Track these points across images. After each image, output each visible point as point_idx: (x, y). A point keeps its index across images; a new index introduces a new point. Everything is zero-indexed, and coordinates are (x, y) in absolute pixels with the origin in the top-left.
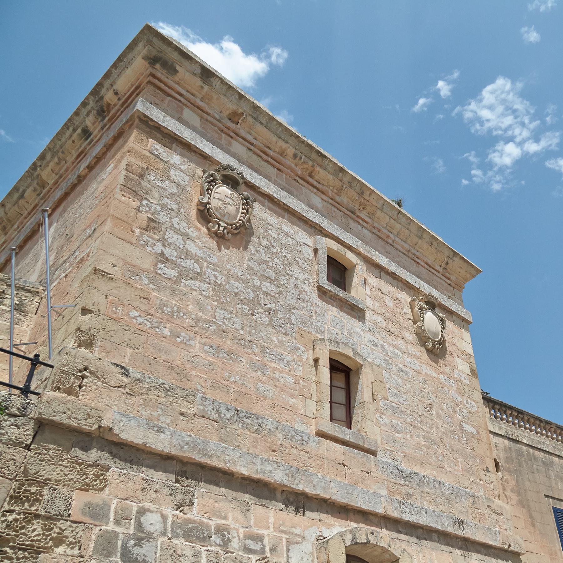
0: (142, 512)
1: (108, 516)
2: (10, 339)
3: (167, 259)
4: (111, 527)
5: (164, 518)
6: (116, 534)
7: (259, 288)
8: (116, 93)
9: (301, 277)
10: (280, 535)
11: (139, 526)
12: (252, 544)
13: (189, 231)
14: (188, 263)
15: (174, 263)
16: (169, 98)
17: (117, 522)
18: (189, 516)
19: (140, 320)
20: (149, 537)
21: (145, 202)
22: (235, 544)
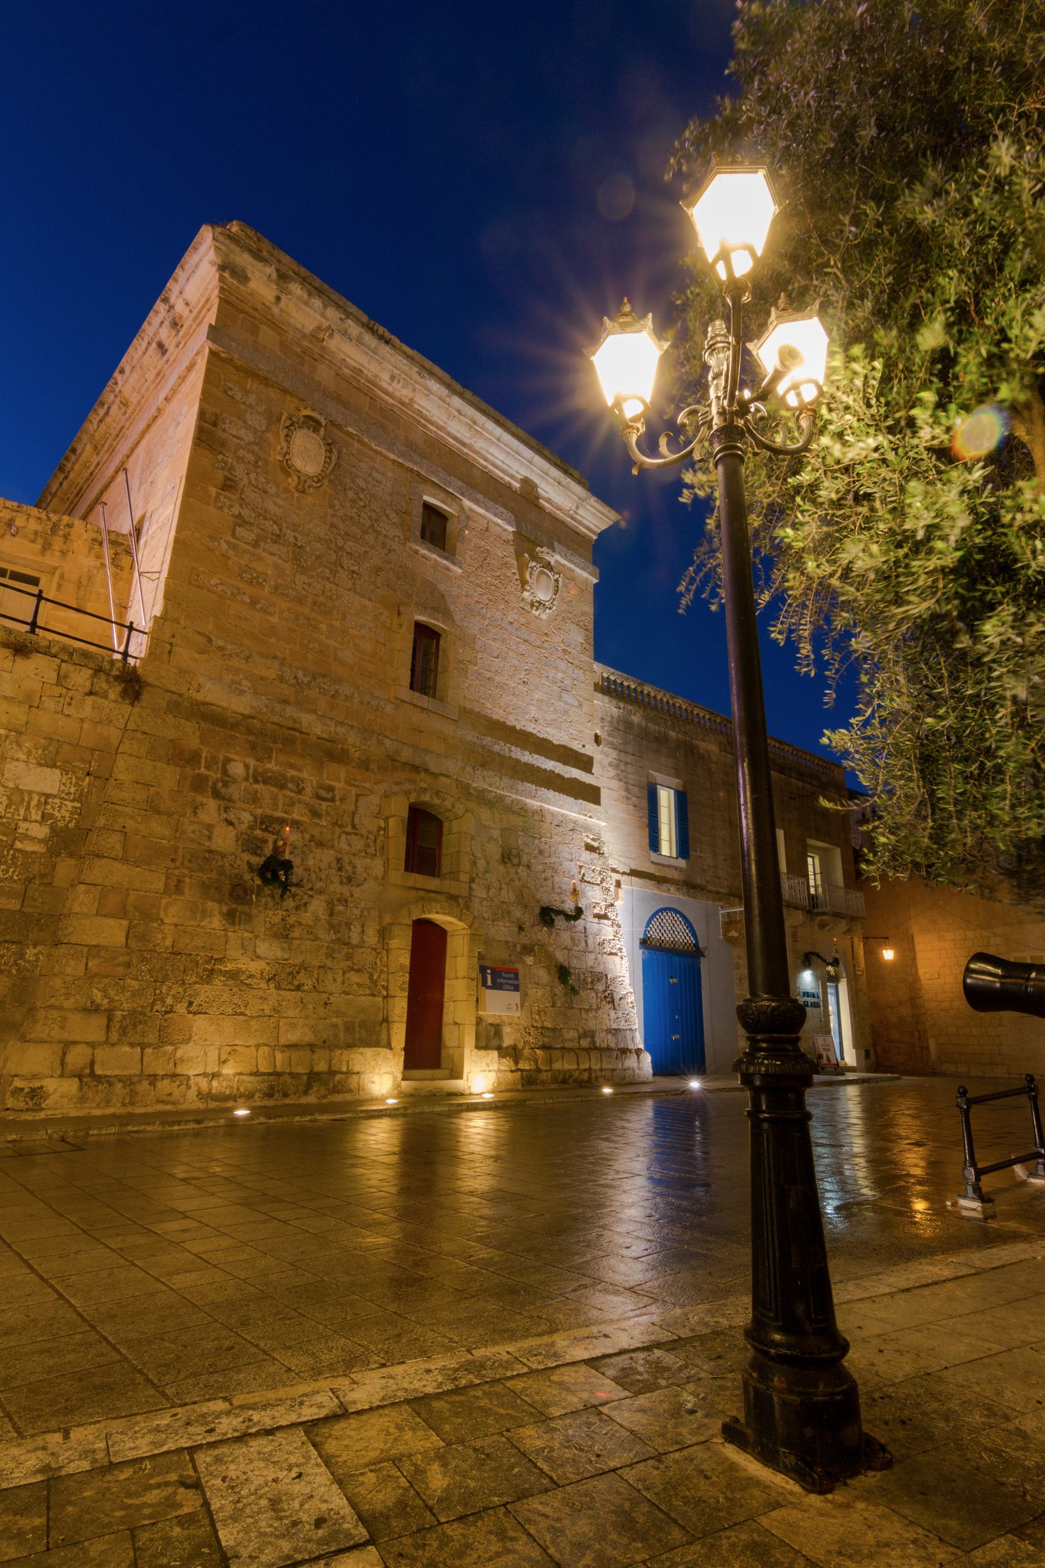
0: (228, 760)
1: (199, 762)
2: (371, 1409)
3: (244, 521)
4: (203, 770)
5: (247, 766)
6: (207, 777)
7: (341, 549)
8: (187, 304)
9: (391, 534)
11: (225, 772)
12: (323, 793)
13: (267, 488)
14: (269, 526)
15: (251, 524)
16: (241, 316)
17: (208, 768)
18: (269, 766)
19: (221, 588)
20: (234, 781)
21: (220, 457)
22: (309, 791)
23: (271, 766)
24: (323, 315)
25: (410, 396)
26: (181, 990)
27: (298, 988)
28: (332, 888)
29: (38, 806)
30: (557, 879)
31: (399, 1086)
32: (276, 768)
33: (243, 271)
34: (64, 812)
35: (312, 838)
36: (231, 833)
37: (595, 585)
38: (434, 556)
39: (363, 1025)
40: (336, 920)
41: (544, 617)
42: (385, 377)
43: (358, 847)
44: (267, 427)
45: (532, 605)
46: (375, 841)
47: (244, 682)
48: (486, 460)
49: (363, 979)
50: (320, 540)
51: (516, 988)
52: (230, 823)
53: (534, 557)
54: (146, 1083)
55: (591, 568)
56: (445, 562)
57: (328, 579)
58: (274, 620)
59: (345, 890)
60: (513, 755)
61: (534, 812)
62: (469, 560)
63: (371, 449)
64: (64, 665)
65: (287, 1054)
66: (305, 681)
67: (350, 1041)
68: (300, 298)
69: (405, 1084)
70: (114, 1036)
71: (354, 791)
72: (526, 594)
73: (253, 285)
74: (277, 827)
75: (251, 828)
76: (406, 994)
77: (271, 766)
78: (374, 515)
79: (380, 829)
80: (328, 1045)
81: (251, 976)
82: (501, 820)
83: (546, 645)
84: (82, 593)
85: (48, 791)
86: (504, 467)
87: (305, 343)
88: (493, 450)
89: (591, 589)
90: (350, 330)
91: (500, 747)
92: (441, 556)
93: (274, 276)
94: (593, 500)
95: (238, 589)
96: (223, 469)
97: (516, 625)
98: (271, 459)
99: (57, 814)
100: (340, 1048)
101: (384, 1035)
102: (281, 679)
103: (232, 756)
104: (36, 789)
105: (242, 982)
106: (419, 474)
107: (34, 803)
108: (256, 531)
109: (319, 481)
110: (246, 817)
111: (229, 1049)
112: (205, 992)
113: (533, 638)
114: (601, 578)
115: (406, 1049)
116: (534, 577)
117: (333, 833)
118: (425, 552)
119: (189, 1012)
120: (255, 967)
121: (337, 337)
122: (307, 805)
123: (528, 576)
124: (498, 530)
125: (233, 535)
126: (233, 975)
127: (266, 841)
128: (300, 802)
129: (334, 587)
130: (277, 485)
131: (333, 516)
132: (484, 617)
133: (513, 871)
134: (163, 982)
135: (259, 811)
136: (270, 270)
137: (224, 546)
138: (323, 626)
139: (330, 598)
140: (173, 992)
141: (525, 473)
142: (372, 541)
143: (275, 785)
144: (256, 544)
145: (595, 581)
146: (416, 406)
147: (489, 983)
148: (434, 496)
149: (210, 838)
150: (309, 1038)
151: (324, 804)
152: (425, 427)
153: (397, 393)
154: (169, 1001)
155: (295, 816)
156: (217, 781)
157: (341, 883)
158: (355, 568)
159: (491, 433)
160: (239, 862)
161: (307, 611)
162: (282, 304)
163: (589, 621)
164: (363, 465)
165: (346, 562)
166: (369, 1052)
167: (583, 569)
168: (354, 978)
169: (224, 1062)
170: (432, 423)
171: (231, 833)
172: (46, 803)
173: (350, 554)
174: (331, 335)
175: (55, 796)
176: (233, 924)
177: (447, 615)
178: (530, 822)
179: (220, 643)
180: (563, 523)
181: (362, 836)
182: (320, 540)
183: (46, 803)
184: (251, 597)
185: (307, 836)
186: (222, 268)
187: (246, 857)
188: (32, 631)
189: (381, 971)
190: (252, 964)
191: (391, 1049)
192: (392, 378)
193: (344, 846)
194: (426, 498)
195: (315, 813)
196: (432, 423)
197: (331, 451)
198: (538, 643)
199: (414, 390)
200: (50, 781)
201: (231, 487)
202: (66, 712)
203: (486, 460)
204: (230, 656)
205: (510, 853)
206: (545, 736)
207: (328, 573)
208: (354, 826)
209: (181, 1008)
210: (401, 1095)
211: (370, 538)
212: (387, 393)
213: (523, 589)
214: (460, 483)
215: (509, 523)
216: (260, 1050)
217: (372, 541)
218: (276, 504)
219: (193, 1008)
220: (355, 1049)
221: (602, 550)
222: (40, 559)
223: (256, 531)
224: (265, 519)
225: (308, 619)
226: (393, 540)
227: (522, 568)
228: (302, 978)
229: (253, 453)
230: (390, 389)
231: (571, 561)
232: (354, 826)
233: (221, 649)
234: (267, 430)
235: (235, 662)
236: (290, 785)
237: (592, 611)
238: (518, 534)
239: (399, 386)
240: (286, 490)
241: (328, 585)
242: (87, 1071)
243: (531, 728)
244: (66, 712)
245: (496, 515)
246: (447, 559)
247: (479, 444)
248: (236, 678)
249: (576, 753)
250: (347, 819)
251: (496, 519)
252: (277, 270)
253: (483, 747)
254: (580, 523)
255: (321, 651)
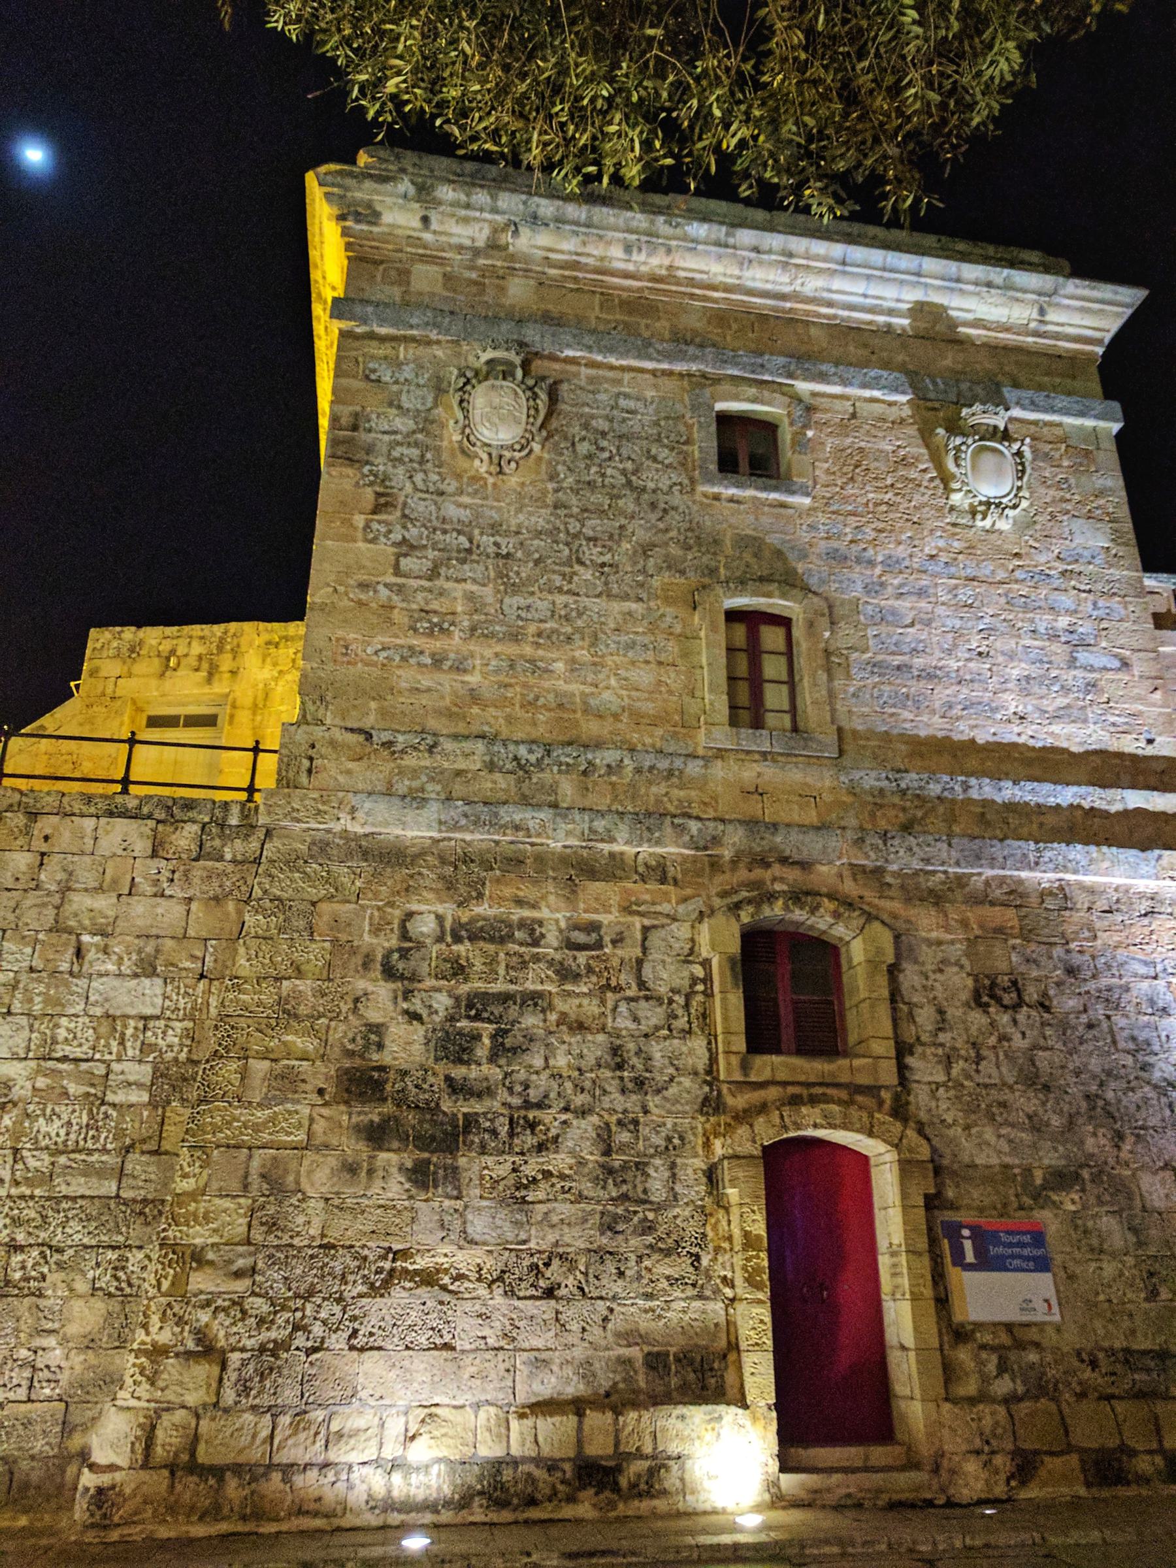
0: (410, 915)
5: (440, 918)
9: (664, 484)
10: (630, 919)
11: (405, 936)
12: (580, 937)
20: (420, 945)
22: (552, 938)
23: (483, 909)
24: (495, 210)
25: (667, 262)
26: (337, 1309)
27: (549, 1293)
28: (606, 1102)
29: (135, 1037)
30: (1119, 1021)
31: (776, 1484)
32: (491, 912)
33: (369, 205)
34: (170, 1039)
35: (563, 1019)
36: (418, 1032)
37: (1120, 437)
38: (750, 493)
39: (684, 1358)
40: (617, 1160)
41: (1004, 525)
42: (617, 252)
43: (654, 1021)
44: (436, 399)
45: (974, 513)
46: (687, 1006)
47: (429, 787)
48: (830, 304)
49: (680, 1267)
50: (538, 534)
51: (1042, 1265)
52: (414, 1017)
53: (954, 427)
54: (276, 1476)
55: (1099, 405)
56: (774, 496)
57: (560, 590)
58: (473, 679)
59: (632, 1102)
60: (974, 794)
61: (1044, 894)
62: (823, 478)
63: (612, 368)
64: (160, 827)
65: (529, 1422)
66: (533, 758)
67: (660, 1389)
68: (455, 204)
69: (790, 1482)
70: (229, 1396)
71: (638, 922)
72: (956, 498)
73: (388, 218)
74: (497, 1010)
75: (451, 1019)
76: (764, 1295)
77: (483, 909)
78: (629, 465)
79: (694, 981)
80: (615, 1401)
81: (460, 1277)
82: (965, 924)
83: (1019, 574)
84: (259, 718)
85: (148, 1011)
86: (769, 287)
87: (481, 262)
88: (837, 284)
89: (1110, 446)
90: (542, 212)
91: (985, 790)
92: (765, 489)
93: (412, 191)
94: (1073, 286)
95: (411, 648)
96: (371, 484)
97: (944, 557)
98: (445, 443)
99: (160, 1041)
100: (635, 1405)
101: (730, 1377)
102: (491, 767)
103: (415, 907)
104: (132, 1012)
105: (444, 1288)
106: (704, 376)
107: (129, 1032)
108: (431, 554)
109: (522, 448)
110: (442, 1002)
111: (423, 1413)
112: (378, 1311)
113: (986, 569)
114: (1127, 417)
115: (783, 1406)
116: (967, 462)
117: (603, 1002)
118: (732, 491)
119: (352, 1348)
120: (465, 1259)
121: (525, 231)
122: (551, 963)
123: (951, 465)
124: (878, 408)
125: (397, 572)
126: (428, 1278)
127: (477, 1037)
128: (537, 958)
129: (571, 599)
130: (458, 477)
131: (556, 491)
132: (871, 563)
133: (1005, 1018)
134: (306, 1299)
135: (464, 989)
136: (405, 186)
137: (384, 592)
138: (559, 666)
139: (567, 618)
140: (323, 1315)
141: (913, 295)
142: (631, 507)
143: (492, 940)
144: (433, 574)
145: (1116, 427)
146: (682, 274)
147: (970, 1257)
148: (736, 398)
149: (380, 1046)
150: (574, 1388)
151: (582, 957)
152: (705, 299)
153: (643, 269)
154: (317, 1330)
155: (530, 986)
156: (390, 952)
157: (623, 1091)
158: (607, 558)
159: (825, 259)
160: (431, 1080)
161: (528, 650)
162: (434, 226)
163: (1117, 500)
164: (602, 397)
165: (592, 553)
166: (697, 1414)
167: (1081, 414)
168: (665, 1268)
169: (413, 1438)
170: (714, 288)
171: (418, 1032)
172: (145, 1028)
173: (595, 539)
174: (516, 232)
175: (158, 1018)
176: (424, 1186)
177: (791, 582)
178: (1038, 918)
179: (386, 736)
180: (1019, 350)
181: (659, 1000)
182: (538, 534)
183: (145, 1028)
184: (432, 656)
185: (553, 1017)
186: (341, 218)
187: (442, 1068)
188: (125, 791)
189: (718, 1250)
190: (460, 1256)
191: (745, 1406)
192: (628, 249)
193: (624, 1023)
194: (720, 406)
195: (565, 974)
196: (714, 288)
197: (535, 396)
198: (1001, 575)
199: (669, 251)
200: (149, 995)
201: (386, 504)
202: (167, 892)
203: (830, 304)
204: (403, 752)
205: (993, 985)
206: (1049, 742)
207: (558, 581)
208: (642, 985)
209: (337, 1341)
210: (778, 1500)
211: (627, 503)
212: (627, 275)
213: (948, 490)
214: (781, 360)
215: (896, 390)
216: (482, 1414)
217: (631, 507)
218: (459, 505)
219: (359, 1341)
220: (666, 1409)
221: (1121, 369)
222: (206, 690)
223: (431, 554)
224: (445, 532)
225: (532, 661)
226: (670, 491)
227: (937, 459)
228: (555, 1272)
229: (417, 444)
230: (631, 267)
231: (1052, 410)
232: (642, 985)
233: (388, 744)
234: (436, 405)
235: (410, 761)
236: (518, 935)
237: (1121, 483)
238: (921, 398)
239: (642, 257)
240: (475, 479)
241: (560, 599)
242: (185, 1457)
243: (1011, 734)
244: (167, 892)
245: (864, 386)
246: (776, 489)
247: (811, 285)
248: (416, 784)
249: (1134, 757)
250: (626, 978)
251: (867, 393)
252: (413, 183)
253: (903, 792)
254: (1057, 336)
255: (561, 706)
